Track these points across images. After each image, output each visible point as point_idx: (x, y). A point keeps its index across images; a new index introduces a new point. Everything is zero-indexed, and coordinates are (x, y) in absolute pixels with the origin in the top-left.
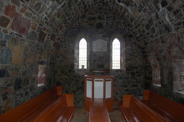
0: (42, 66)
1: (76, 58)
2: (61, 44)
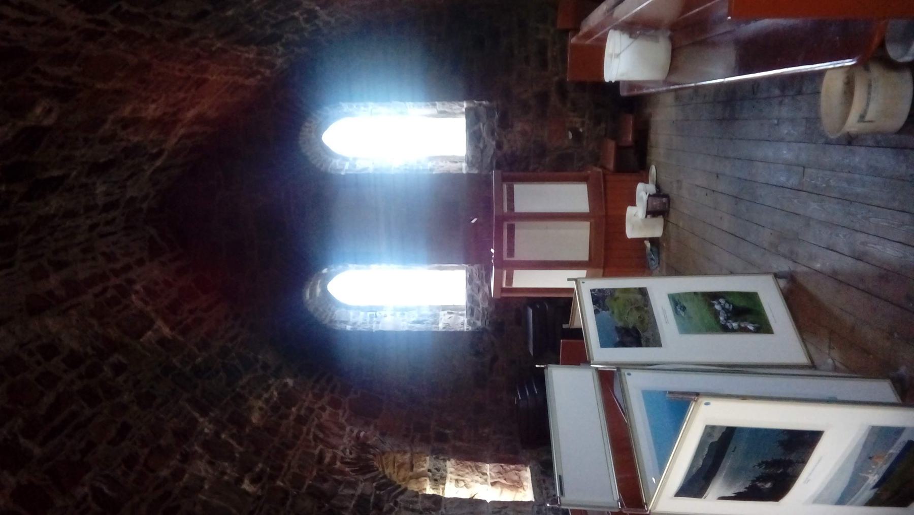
0: (449, 476)
1: (418, 322)
2: (356, 393)
